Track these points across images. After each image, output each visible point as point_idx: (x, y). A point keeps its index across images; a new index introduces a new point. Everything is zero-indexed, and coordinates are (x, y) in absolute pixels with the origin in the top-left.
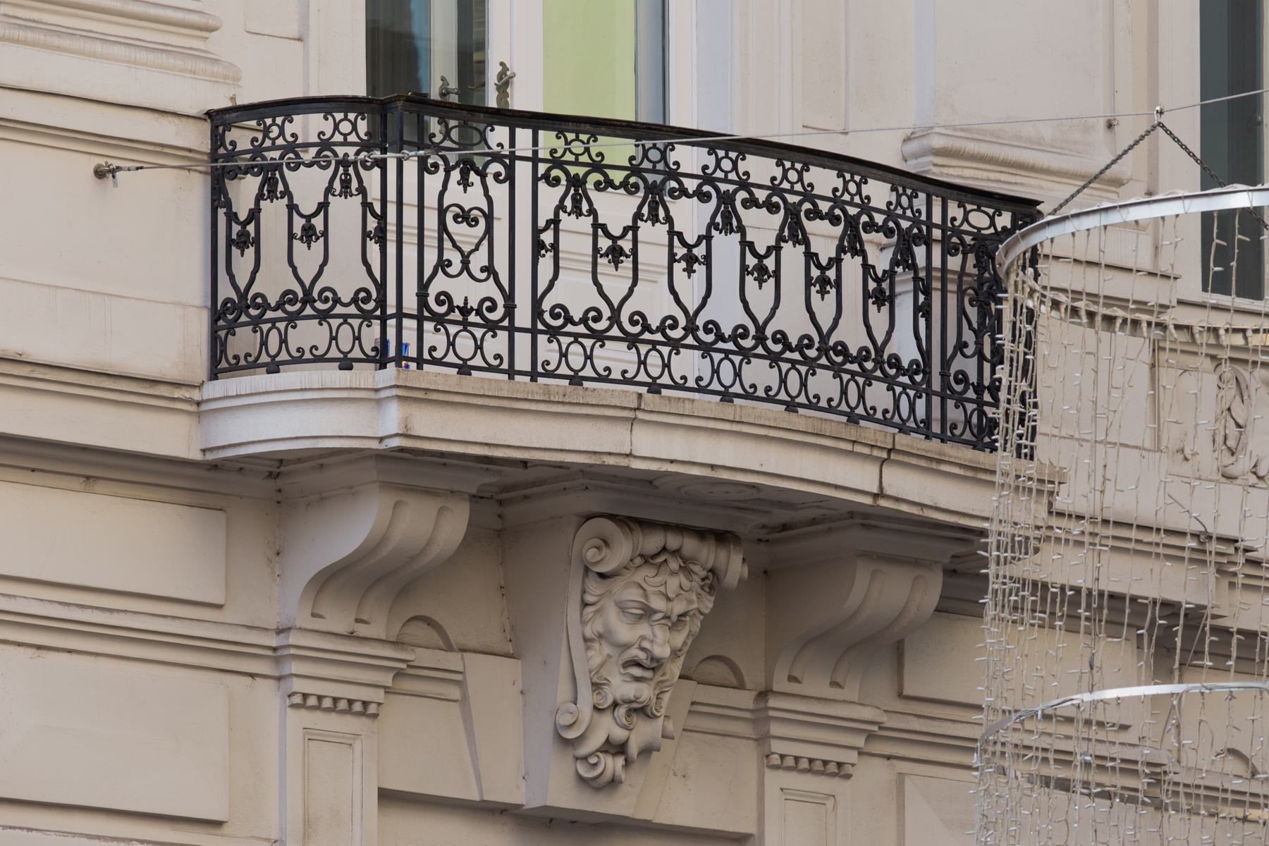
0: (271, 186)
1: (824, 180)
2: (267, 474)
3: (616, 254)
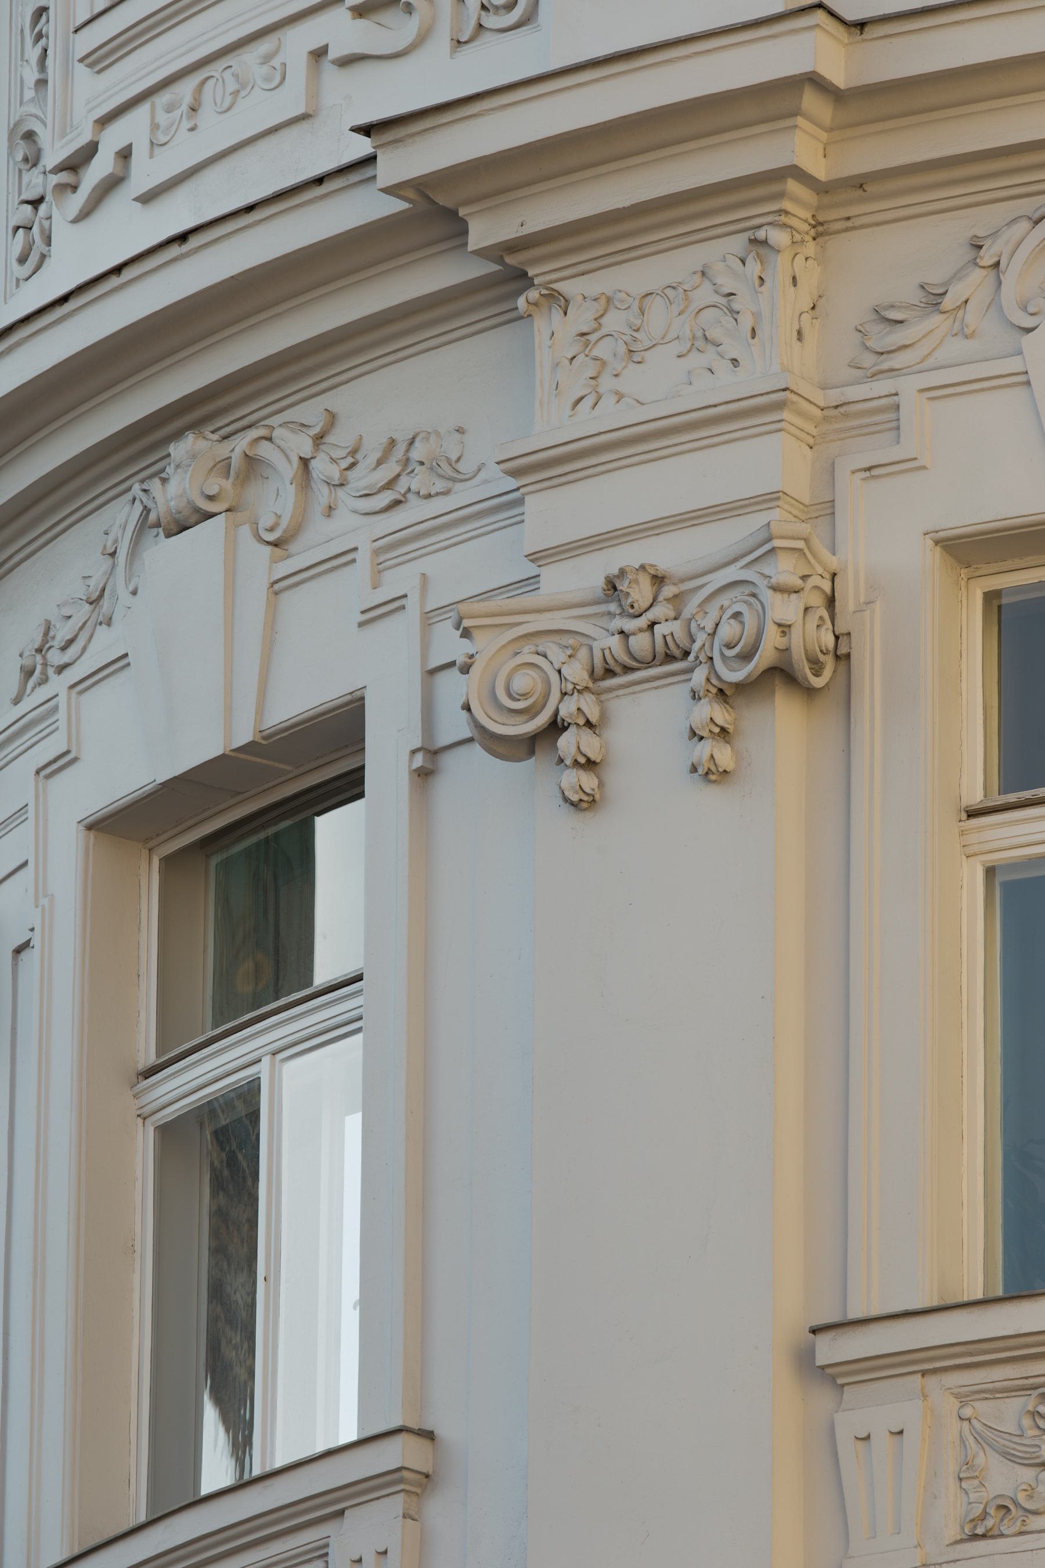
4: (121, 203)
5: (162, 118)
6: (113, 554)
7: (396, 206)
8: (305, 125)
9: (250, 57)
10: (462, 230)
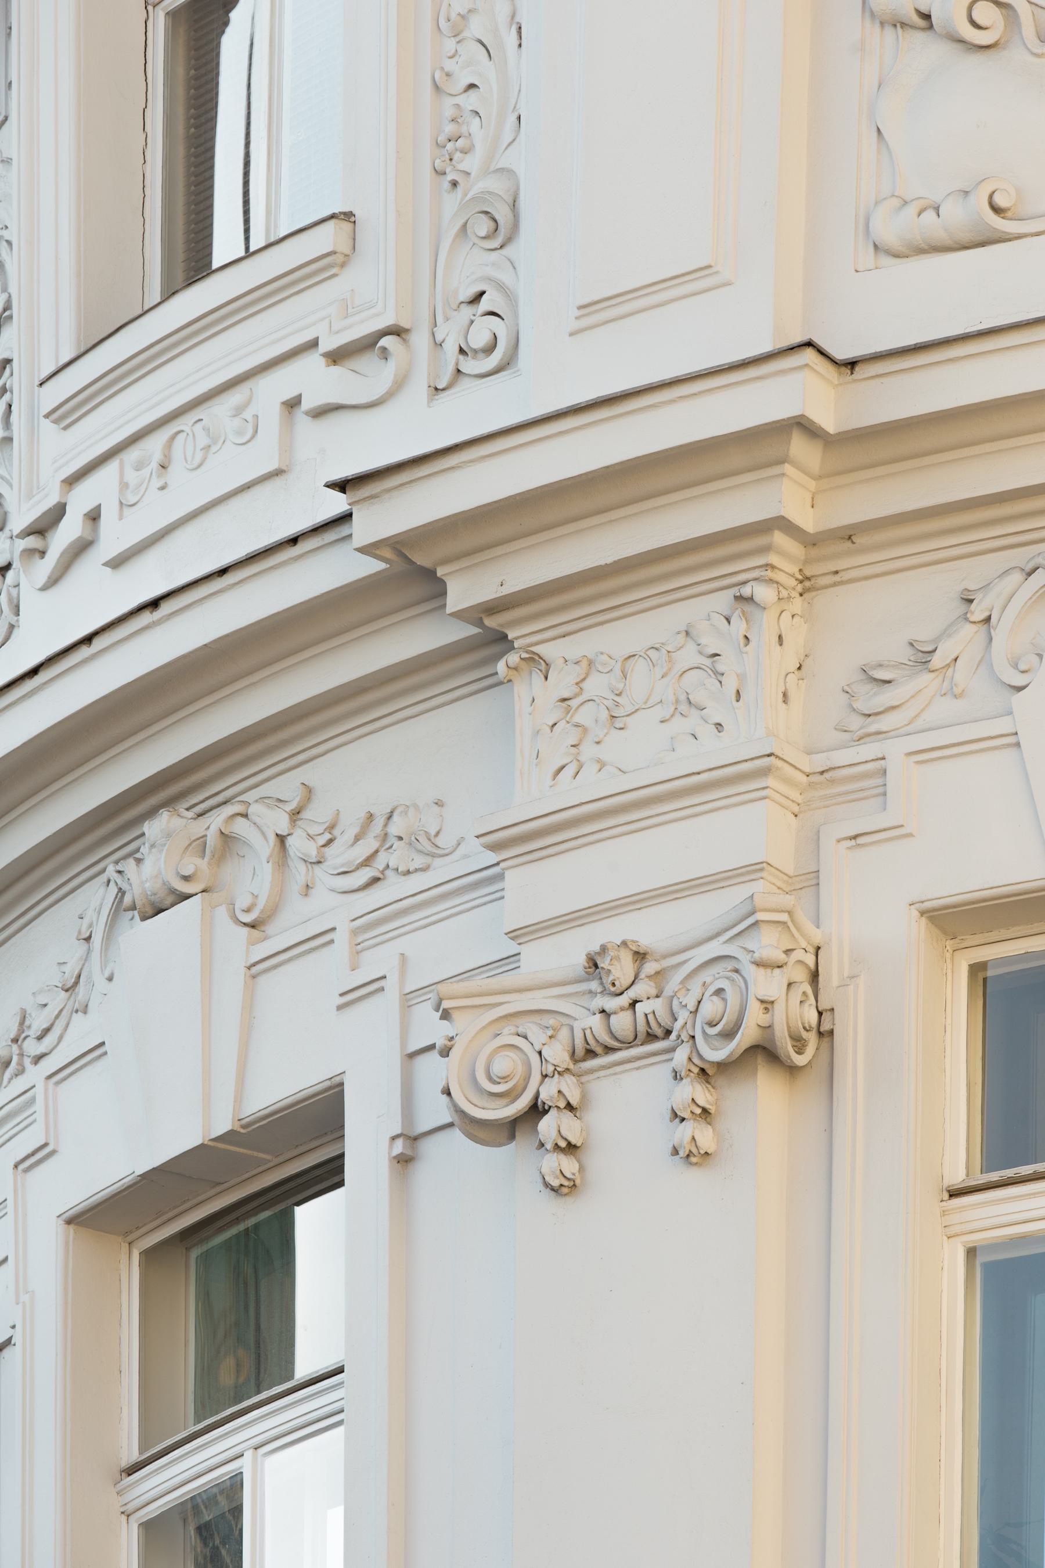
4: (92, 564)
5: (131, 477)
6: (88, 939)
7: (373, 566)
8: (278, 482)
9: (221, 409)
10: (441, 592)
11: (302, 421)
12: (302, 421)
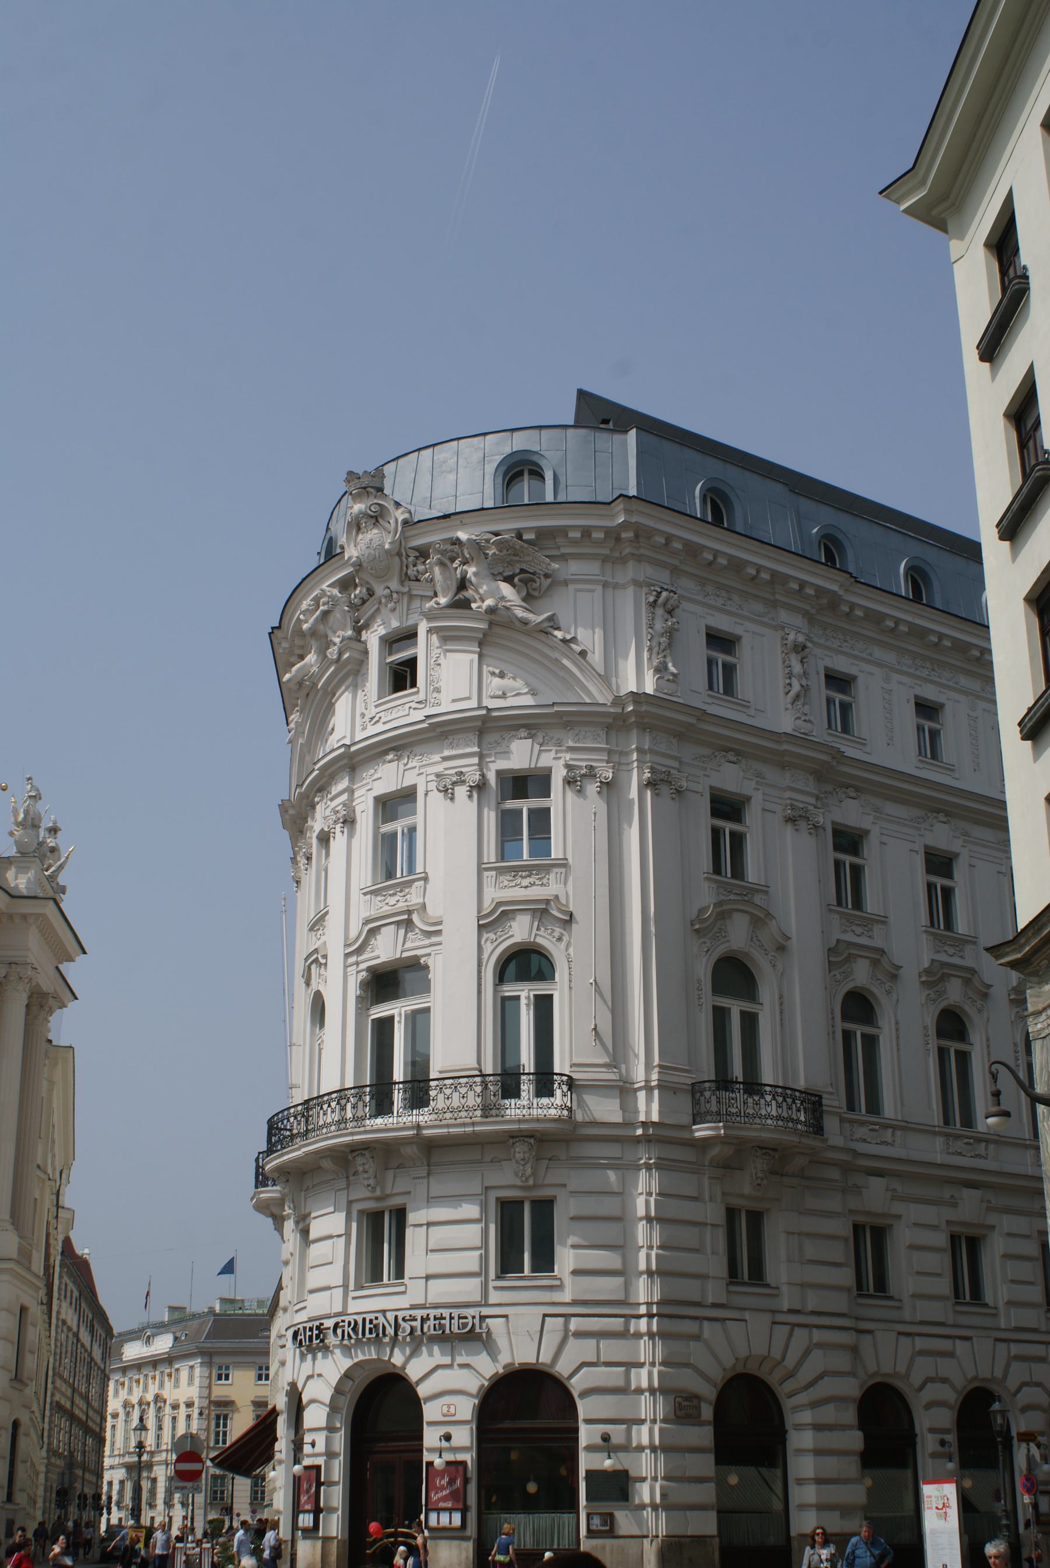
0: (702, 1094)
1: (789, 1092)
2: (36, 823)
3: (757, 1104)
4: (380, 724)
11: (411, 710)
12: (411, 710)
